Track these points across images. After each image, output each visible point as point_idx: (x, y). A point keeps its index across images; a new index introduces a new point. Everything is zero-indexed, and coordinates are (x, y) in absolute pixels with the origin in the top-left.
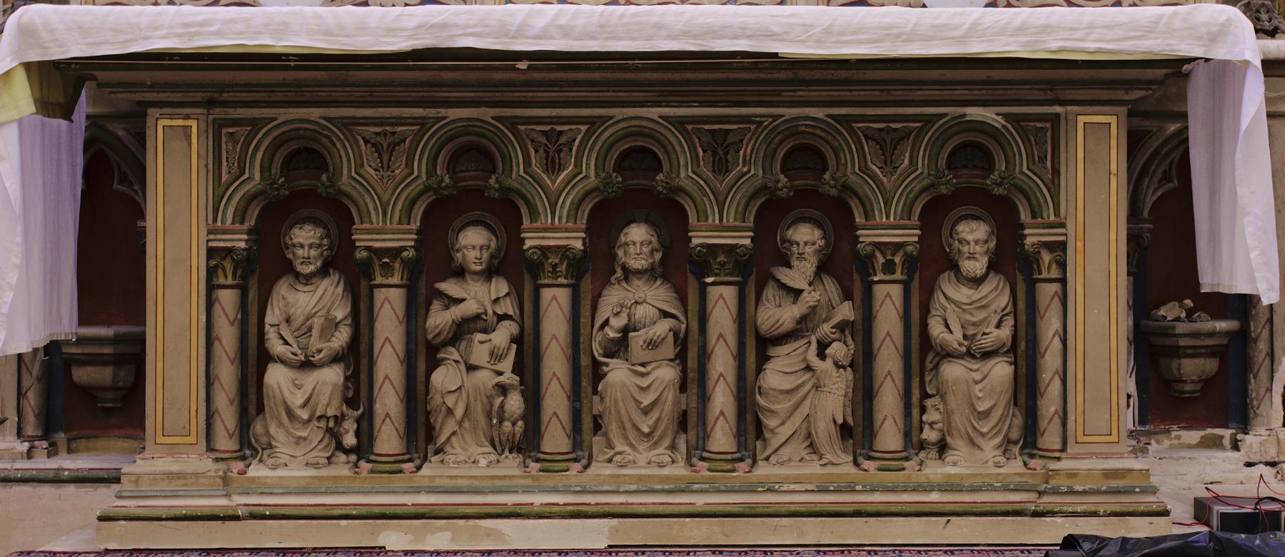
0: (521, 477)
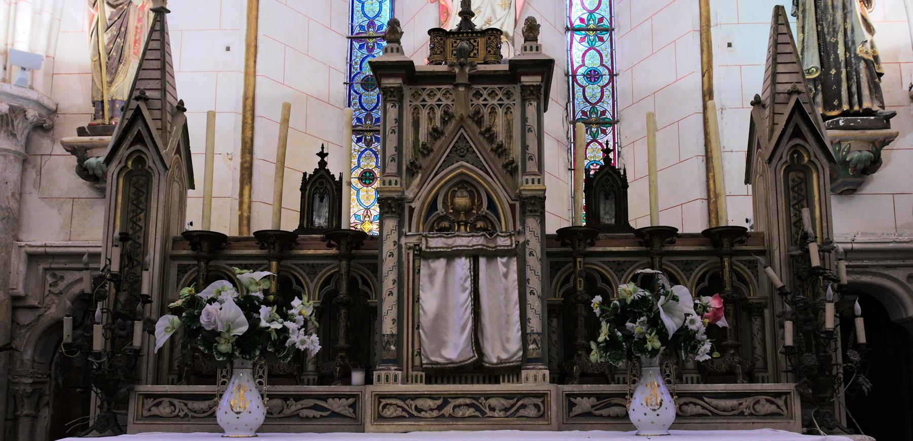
0: (416, 139)
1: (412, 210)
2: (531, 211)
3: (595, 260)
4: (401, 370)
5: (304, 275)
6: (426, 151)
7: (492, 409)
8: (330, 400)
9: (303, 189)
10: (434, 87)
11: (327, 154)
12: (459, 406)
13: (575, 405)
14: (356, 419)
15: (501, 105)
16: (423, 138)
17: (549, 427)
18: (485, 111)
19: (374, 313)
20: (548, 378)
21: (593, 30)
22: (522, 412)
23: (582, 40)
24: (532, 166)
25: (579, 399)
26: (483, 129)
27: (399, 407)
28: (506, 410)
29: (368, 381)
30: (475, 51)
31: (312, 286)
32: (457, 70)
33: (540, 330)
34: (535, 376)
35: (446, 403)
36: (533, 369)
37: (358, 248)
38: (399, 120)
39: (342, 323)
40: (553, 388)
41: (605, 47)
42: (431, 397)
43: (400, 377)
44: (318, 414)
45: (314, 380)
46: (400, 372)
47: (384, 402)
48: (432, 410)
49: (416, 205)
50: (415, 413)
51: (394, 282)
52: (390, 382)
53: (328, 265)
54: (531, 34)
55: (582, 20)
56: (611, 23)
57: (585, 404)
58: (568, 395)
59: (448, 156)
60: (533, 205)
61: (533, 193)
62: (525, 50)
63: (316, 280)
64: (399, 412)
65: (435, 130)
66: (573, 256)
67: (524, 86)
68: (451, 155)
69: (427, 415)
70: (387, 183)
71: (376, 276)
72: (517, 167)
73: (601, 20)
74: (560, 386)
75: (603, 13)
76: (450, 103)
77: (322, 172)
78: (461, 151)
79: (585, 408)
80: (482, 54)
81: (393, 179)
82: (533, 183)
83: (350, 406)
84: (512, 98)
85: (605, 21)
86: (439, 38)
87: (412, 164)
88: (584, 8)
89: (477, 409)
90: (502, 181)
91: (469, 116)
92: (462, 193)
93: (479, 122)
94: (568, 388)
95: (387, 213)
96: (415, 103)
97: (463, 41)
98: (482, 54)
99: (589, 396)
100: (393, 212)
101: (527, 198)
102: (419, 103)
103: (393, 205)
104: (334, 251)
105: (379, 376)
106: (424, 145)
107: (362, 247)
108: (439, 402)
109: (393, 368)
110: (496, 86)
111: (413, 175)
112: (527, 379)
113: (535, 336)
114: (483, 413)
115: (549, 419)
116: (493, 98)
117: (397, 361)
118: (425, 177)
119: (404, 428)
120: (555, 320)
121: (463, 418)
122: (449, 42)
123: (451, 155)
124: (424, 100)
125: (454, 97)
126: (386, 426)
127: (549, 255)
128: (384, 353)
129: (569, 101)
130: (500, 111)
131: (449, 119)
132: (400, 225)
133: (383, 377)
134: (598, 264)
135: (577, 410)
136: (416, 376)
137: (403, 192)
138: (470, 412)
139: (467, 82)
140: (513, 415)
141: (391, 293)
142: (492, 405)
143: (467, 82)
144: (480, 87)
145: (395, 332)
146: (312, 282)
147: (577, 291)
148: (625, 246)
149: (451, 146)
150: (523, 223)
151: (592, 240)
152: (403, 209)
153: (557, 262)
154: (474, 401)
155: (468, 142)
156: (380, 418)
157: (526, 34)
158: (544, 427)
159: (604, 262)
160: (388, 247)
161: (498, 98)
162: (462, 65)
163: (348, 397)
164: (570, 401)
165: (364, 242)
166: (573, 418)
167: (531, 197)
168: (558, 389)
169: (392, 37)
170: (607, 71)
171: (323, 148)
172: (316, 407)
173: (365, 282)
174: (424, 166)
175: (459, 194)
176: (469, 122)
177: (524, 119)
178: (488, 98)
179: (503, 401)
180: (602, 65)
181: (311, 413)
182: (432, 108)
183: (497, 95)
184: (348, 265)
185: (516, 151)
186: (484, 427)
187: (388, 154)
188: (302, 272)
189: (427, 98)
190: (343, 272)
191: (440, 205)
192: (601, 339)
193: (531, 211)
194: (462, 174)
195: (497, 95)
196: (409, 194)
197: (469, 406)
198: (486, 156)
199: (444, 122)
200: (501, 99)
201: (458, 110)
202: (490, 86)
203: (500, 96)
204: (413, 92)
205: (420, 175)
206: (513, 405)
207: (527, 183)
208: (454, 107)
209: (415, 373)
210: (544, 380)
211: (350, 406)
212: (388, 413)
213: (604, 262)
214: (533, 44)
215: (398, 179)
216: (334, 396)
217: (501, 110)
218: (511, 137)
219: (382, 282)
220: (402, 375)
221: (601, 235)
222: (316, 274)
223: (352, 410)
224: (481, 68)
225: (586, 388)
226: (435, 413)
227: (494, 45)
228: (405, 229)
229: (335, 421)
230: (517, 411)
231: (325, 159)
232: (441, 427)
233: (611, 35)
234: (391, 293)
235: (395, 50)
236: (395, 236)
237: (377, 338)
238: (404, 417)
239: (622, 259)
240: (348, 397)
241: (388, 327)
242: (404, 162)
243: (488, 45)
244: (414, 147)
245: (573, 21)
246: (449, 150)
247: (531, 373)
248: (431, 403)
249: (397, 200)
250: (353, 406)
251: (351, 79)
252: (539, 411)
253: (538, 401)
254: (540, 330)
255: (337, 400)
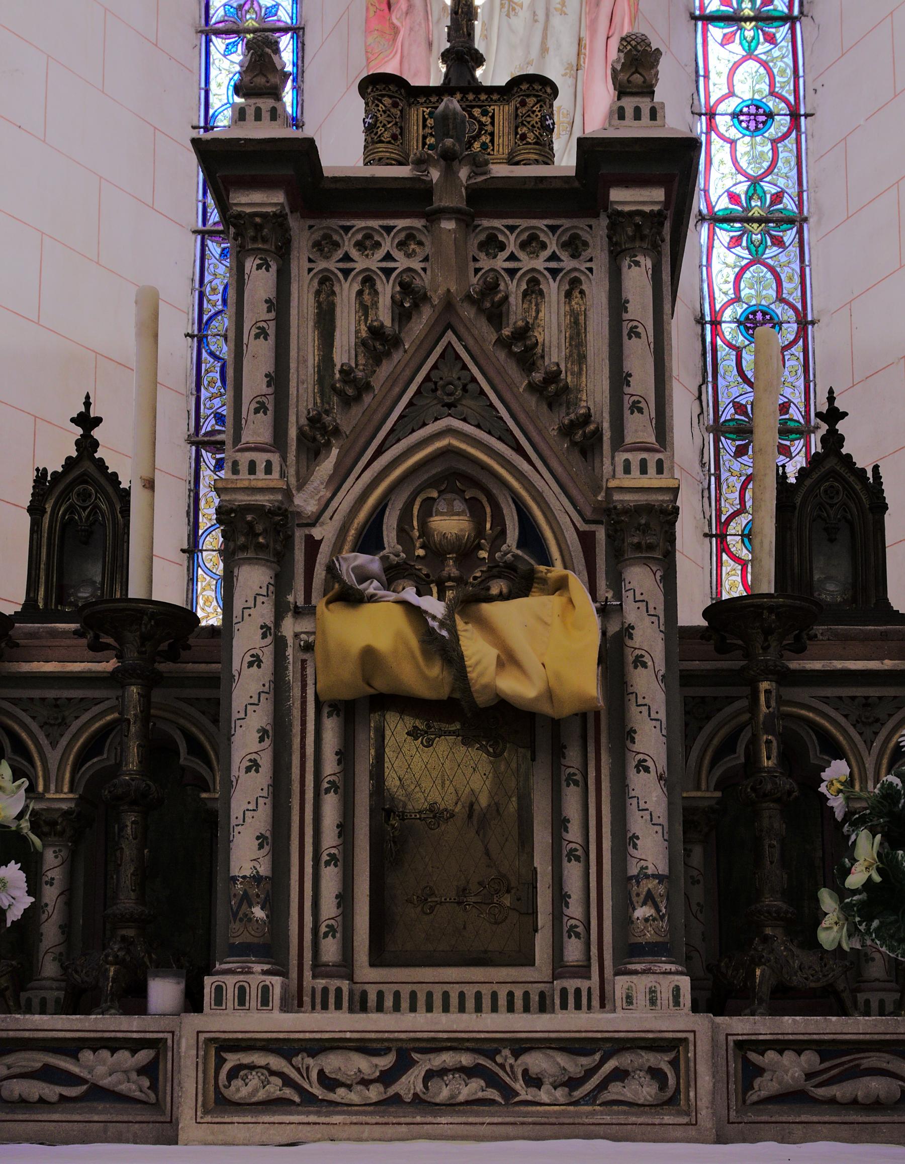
0: (326, 360)
1: (313, 546)
2: (638, 547)
3: (803, 694)
4: (284, 974)
5: (34, 726)
6: (347, 388)
7: (534, 1082)
8: (87, 1056)
9: (35, 509)
10: (375, 223)
11: (98, 421)
12: (442, 1072)
13: (760, 1071)
14: (157, 1106)
15: (554, 272)
16: (343, 354)
17: (692, 1132)
18: (512, 286)
19: (212, 827)
20: (686, 998)
21: (760, 221)
22: (616, 1091)
23: (735, 242)
24: (639, 428)
25: (771, 1055)
26: (506, 332)
27: (273, 1073)
28: (572, 1083)
29: (193, 1002)
30: (485, 139)
31: (53, 757)
32: (435, 175)
33: (663, 869)
34: (652, 991)
35: (404, 1063)
36: (644, 972)
37: (173, 655)
38: (280, 305)
39: (128, 850)
40: (702, 1023)
41: (785, 259)
42: (365, 1046)
43: (277, 992)
44: (52, 1092)
45: (57, 1001)
46: (277, 981)
47: (232, 1060)
48: (366, 1083)
49: (325, 532)
50: (317, 1091)
51: (263, 734)
52: (247, 1007)
53: (97, 702)
54: (637, 79)
55: (733, 198)
56: (800, 205)
57: (790, 1069)
58: (743, 1045)
59: (410, 404)
60: (644, 529)
61: (641, 498)
62: (622, 117)
63: (64, 742)
64: (275, 1088)
65: (376, 332)
66: (747, 681)
67: (620, 214)
68: (420, 402)
69: (353, 1097)
70: (244, 467)
71: (216, 721)
72: (597, 434)
73: (777, 198)
74: (719, 1019)
75: (781, 182)
76: (417, 265)
77: (87, 466)
78: (449, 390)
79: (787, 1078)
80: (503, 143)
81: (261, 459)
82: (644, 470)
83: (142, 1071)
84: (586, 255)
85: (786, 200)
86: (387, 101)
87: (314, 421)
88: (739, 170)
89: (492, 1080)
90: (559, 470)
91: (468, 297)
92: (450, 504)
93: (496, 315)
94: (741, 1026)
95: (244, 548)
96: (322, 265)
97: (449, 117)
98: (503, 143)
99: (798, 1046)
100: (260, 547)
101: (626, 511)
102: (332, 265)
103: (259, 528)
104: (110, 666)
105: (219, 990)
106: (346, 372)
107: (184, 654)
108: (386, 1062)
109: (257, 968)
110: (541, 223)
111: (317, 454)
112: (629, 999)
113: (651, 884)
114: (508, 1093)
115: (690, 1111)
116: (535, 254)
117: (271, 949)
118: (349, 461)
119: (288, 1133)
120: (698, 851)
121: (451, 1106)
122: (416, 114)
123: (420, 402)
124: (347, 258)
125: (428, 249)
126: (238, 1126)
127: (687, 679)
128: (236, 926)
129: (704, 381)
130: (553, 289)
131: (416, 306)
132: (281, 585)
133: (230, 994)
134: (811, 706)
135: (765, 1086)
136: (325, 990)
137: (288, 494)
138: (473, 1088)
139: (463, 205)
140: (591, 1098)
141: (254, 766)
142: (534, 1070)
143: (463, 205)
144: (497, 223)
145: (264, 869)
146: (54, 745)
147: (761, 769)
148: (881, 659)
149: (419, 378)
150: (616, 582)
151: (798, 638)
152: (289, 541)
153: (703, 699)
154: (482, 1061)
155: (465, 367)
156: (220, 1104)
157: (623, 77)
158: (679, 1132)
159: (826, 700)
160: (247, 640)
161: (547, 253)
162: (449, 158)
163: (134, 1045)
164: (746, 1062)
165: (191, 641)
166: (754, 1106)
167: (640, 510)
168: (715, 1028)
169: (260, 81)
170: (791, 313)
171: (87, 404)
172: (47, 1074)
173: (196, 749)
174: (346, 428)
175: (442, 506)
176: (468, 312)
177: (618, 305)
178: (521, 255)
179: (562, 1059)
180: (780, 299)
181: (35, 1089)
182: (368, 280)
183: (544, 246)
184: (145, 697)
185: (595, 391)
186: (510, 1129)
187: (248, 394)
188: (28, 720)
189: (354, 253)
190: (131, 714)
191: (390, 536)
192: (856, 879)
193: (638, 547)
194: (448, 451)
195: (544, 246)
196: (306, 502)
197: (469, 1072)
198: (515, 406)
199: (402, 315)
200: (554, 257)
201: (439, 282)
202: (524, 223)
203: (553, 247)
204: (317, 236)
205: (335, 452)
206: (590, 1073)
207: (627, 470)
208: (427, 278)
209: (321, 983)
210: (677, 1003)
211: (142, 1071)
212: (241, 1090)
213: (826, 700)
214: (645, 104)
215: (275, 458)
216: (98, 1044)
217: (554, 286)
218: (582, 358)
219: (229, 737)
220: (285, 988)
221: (818, 629)
222: (64, 724)
223: (146, 1083)
224: (500, 170)
225: (791, 1025)
226: (374, 1093)
227: (535, 119)
228: (296, 596)
229: (100, 1113)
230: (603, 1086)
231: (96, 433)
232: (390, 1130)
233: (800, 232)
234: (254, 766)
235: (266, 115)
236: (264, 613)
237: (220, 886)
238: (289, 1102)
239: (873, 692)
240: (134, 1045)
241: (245, 856)
242: (292, 418)
243: (518, 122)
244: (321, 381)
245: (713, 199)
246: (413, 388)
247: (642, 983)
248: (363, 1064)
249: (271, 513)
250: (150, 1070)
251: (203, 325)
252: (663, 1086)
253: (661, 1061)
254: (663, 869)
255: (105, 1054)
